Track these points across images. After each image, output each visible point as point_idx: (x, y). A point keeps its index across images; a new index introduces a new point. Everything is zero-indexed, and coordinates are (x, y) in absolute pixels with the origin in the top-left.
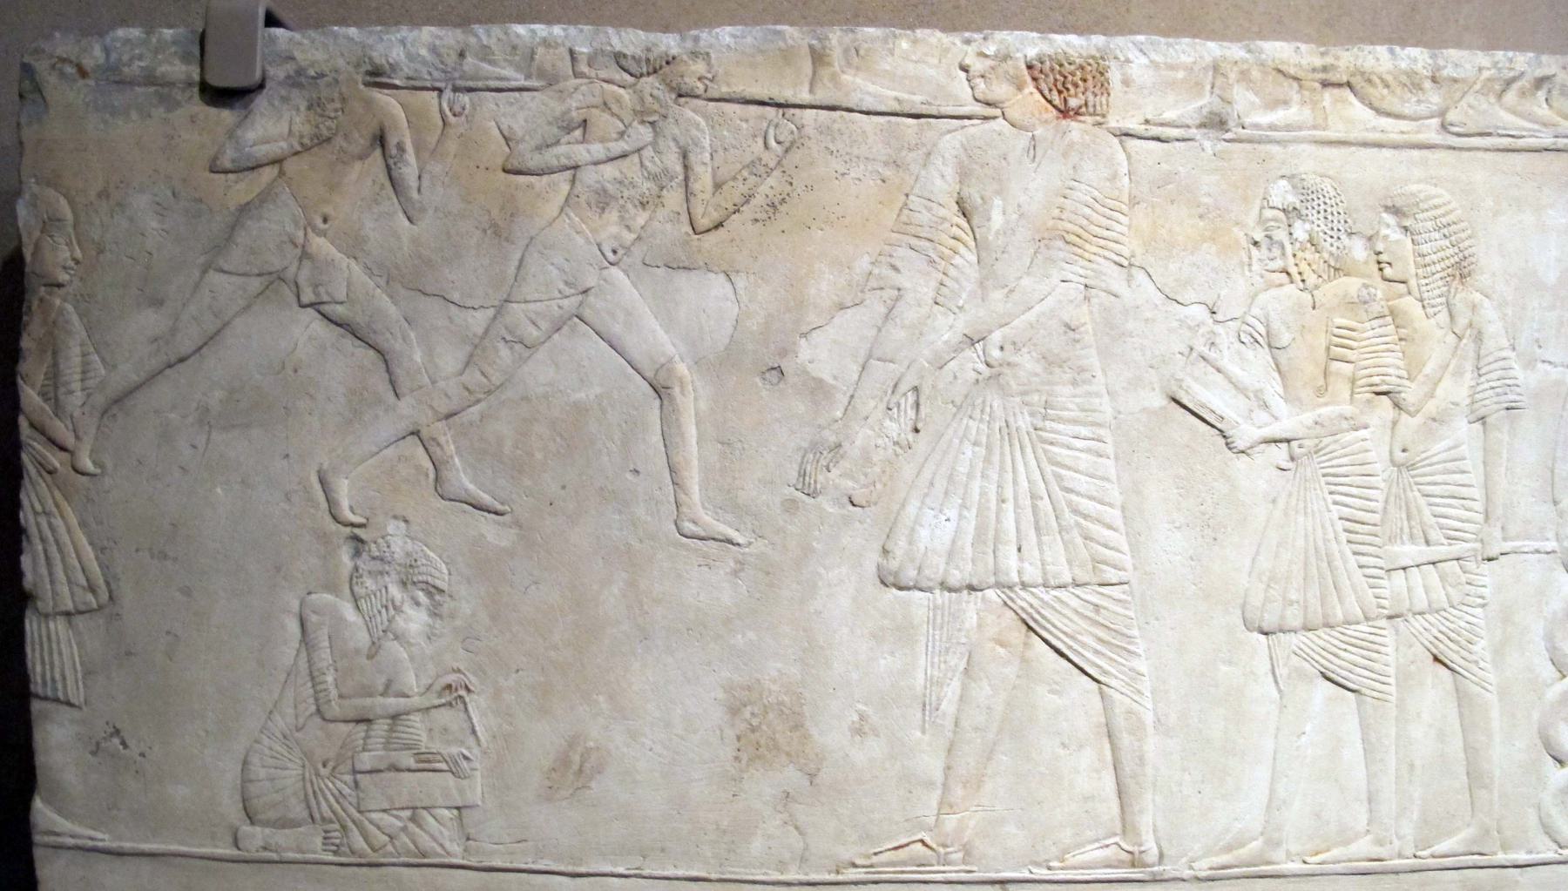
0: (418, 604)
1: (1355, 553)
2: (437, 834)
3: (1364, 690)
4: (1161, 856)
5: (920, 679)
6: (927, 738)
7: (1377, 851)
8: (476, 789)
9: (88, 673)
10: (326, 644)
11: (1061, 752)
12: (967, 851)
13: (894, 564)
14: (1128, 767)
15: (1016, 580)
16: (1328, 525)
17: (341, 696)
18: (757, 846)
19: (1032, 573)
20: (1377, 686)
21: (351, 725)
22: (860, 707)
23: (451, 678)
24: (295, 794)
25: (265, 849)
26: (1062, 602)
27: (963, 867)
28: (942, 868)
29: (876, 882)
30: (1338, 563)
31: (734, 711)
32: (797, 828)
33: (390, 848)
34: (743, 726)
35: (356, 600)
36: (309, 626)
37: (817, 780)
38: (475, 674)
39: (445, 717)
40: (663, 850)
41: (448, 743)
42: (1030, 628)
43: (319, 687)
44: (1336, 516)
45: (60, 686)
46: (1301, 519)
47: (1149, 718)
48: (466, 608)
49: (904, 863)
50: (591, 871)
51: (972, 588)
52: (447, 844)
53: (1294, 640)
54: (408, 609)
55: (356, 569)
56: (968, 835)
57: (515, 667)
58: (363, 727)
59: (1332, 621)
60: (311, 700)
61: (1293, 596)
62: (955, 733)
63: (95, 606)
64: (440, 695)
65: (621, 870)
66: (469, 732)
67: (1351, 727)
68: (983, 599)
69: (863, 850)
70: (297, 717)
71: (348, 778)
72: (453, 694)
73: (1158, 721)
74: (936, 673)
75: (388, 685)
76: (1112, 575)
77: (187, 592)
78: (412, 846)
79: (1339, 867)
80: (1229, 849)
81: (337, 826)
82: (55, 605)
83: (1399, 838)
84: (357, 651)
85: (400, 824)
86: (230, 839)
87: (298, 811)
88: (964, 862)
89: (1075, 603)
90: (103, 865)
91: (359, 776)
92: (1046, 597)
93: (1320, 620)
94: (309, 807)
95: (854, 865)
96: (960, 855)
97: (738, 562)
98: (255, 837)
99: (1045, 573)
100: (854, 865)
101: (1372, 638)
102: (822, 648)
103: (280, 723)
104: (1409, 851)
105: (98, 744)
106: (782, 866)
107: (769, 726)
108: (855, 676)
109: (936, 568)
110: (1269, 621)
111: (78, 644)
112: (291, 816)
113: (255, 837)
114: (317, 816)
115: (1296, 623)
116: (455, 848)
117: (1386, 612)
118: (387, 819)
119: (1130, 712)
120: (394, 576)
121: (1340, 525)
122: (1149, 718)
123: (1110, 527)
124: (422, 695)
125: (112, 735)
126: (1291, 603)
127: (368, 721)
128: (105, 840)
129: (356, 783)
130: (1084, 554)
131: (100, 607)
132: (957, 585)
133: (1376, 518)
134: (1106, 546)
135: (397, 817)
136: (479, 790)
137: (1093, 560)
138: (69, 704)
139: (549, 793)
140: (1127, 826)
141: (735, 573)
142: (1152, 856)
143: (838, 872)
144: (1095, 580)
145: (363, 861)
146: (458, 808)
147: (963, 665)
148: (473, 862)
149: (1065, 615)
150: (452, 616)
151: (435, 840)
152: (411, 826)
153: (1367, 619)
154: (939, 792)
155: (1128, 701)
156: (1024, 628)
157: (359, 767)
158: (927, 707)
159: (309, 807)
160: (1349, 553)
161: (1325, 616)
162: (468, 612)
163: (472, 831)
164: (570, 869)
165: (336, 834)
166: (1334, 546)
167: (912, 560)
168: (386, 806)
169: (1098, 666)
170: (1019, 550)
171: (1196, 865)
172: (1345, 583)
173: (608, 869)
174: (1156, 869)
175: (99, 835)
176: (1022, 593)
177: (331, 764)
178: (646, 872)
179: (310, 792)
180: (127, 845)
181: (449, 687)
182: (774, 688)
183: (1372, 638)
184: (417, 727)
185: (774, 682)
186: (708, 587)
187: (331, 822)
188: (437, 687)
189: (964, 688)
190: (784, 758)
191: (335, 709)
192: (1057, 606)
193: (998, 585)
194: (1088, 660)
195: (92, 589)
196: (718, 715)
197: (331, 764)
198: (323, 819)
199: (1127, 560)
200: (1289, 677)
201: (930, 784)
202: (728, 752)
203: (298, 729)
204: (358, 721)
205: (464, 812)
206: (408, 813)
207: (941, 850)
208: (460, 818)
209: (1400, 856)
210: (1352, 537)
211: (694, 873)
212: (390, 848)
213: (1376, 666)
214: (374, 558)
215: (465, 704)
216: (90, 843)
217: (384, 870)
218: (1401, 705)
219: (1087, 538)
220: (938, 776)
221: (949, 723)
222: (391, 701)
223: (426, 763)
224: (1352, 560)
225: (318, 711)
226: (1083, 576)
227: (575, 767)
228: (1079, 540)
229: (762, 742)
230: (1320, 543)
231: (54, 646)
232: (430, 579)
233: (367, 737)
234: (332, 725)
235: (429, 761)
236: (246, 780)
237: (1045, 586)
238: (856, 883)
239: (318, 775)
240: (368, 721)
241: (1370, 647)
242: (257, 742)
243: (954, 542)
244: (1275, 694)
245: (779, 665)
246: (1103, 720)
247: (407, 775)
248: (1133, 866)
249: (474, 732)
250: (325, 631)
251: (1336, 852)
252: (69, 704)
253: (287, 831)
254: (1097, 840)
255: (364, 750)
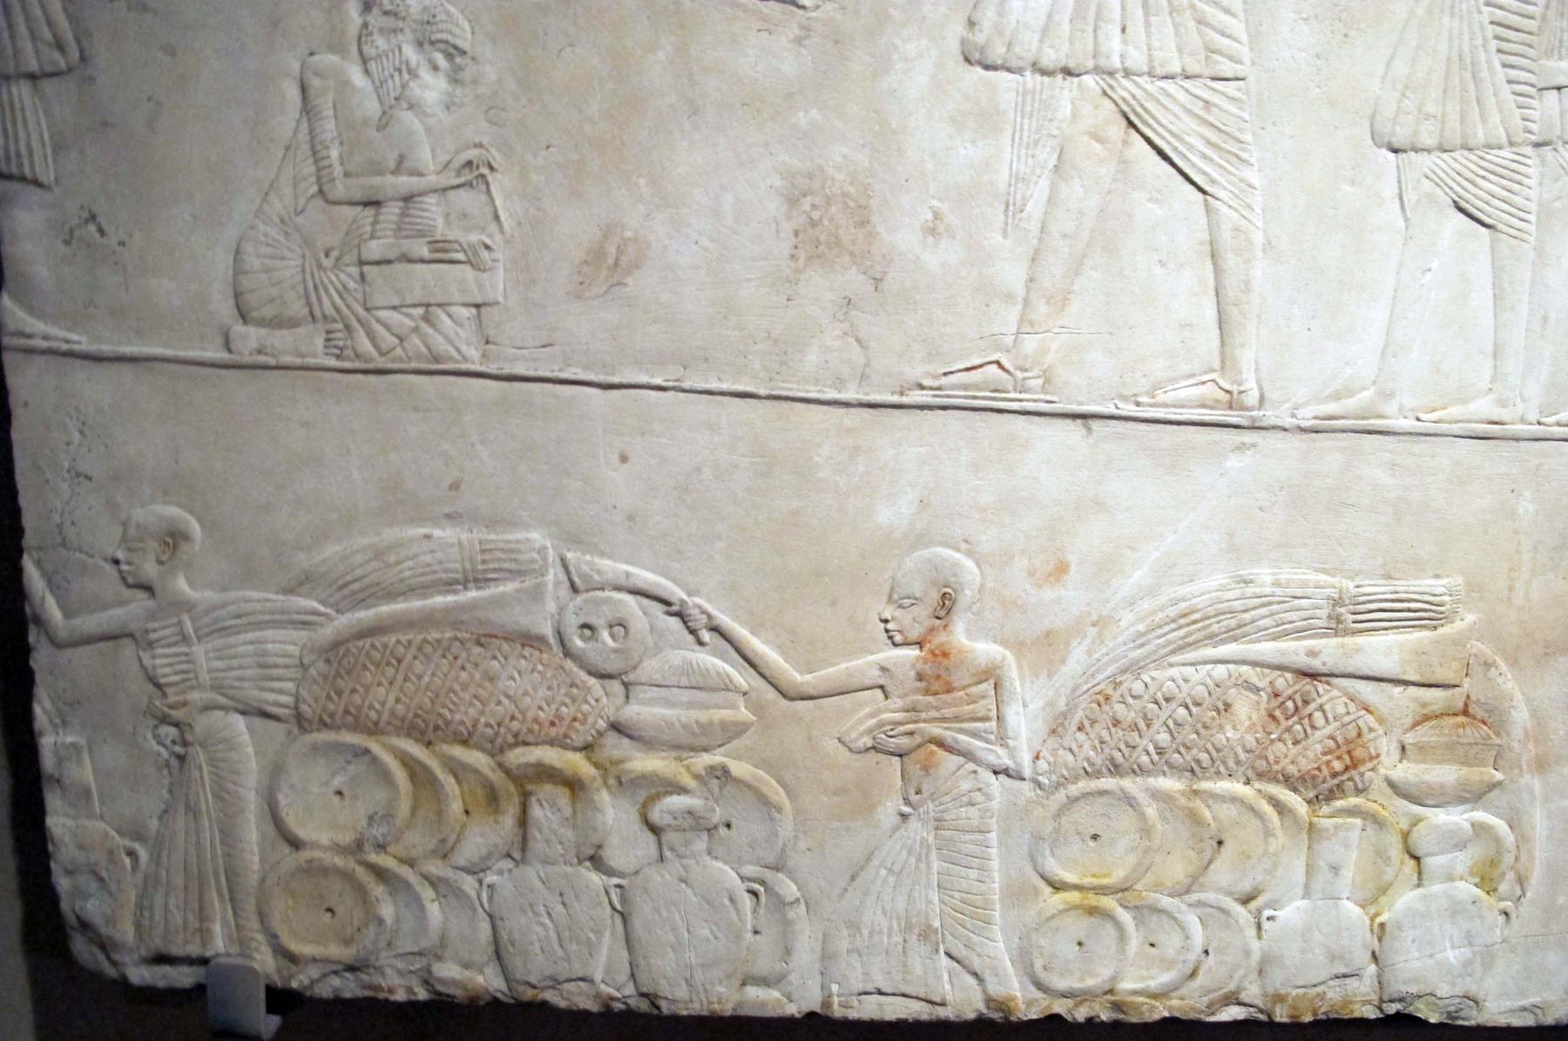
0: (435, 68)
1: (1504, 66)
2: (452, 335)
3: (1500, 226)
4: (1262, 399)
5: (1004, 175)
6: (1008, 243)
7: (1503, 414)
8: (497, 284)
9: (57, 150)
10: (331, 112)
11: (1158, 270)
12: (1048, 380)
13: (980, 38)
14: (1231, 293)
15: (1118, 65)
16: (1477, 30)
17: (347, 175)
18: (812, 358)
19: (1137, 60)
20: (1515, 222)
21: (360, 208)
22: (935, 203)
23: (472, 154)
24: (293, 287)
25: (260, 352)
26: (1169, 95)
27: (1042, 397)
28: (1019, 396)
29: (944, 408)
30: (1485, 74)
31: (792, 202)
32: (858, 340)
33: (399, 351)
34: (803, 219)
35: (365, 61)
36: (312, 92)
37: (884, 286)
38: (499, 150)
39: (465, 199)
40: (706, 360)
41: (468, 230)
42: (1131, 124)
43: (322, 164)
44: (1486, 20)
45: (26, 162)
46: (1446, 20)
47: (1258, 238)
48: (490, 73)
49: (977, 387)
50: (625, 381)
51: (1068, 72)
52: (464, 348)
53: (1425, 162)
54: (426, 75)
55: (365, 25)
56: (1049, 359)
57: (545, 144)
58: (370, 211)
59: (1472, 143)
60: (313, 179)
61: (1430, 108)
62: (1040, 240)
63: (63, 65)
64: (459, 173)
65: (658, 381)
66: (490, 217)
67: (1482, 270)
68: (1080, 86)
69: (930, 368)
70: (296, 198)
71: (354, 270)
72: (474, 174)
73: (1268, 245)
74: (1023, 169)
75: (401, 159)
76: (1227, 68)
77: (171, 51)
78: (423, 349)
79: (1455, 428)
80: (1337, 396)
81: (340, 326)
82: (17, 65)
83: (1523, 400)
84: (365, 123)
85: (412, 324)
86: (220, 341)
87: (297, 308)
88: (1044, 390)
89: (1182, 97)
90: (80, 374)
91: (366, 268)
92: (1149, 87)
93: (1458, 141)
94: (309, 304)
95: (922, 387)
96: (1040, 382)
97: (801, 27)
98: (250, 338)
99: (1151, 60)
100: (922, 387)
101: (1514, 166)
102: (894, 132)
103: (277, 206)
104: (1533, 417)
105: (71, 231)
106: (840, 383)
107: (831, 220)
108: (930, 166)
109: (1029, 45)
110: (1401, 137)
111: (46, 112)
112: (290, 313)
113: (250, 338)
114: (317, 313)
115: (1429, 141)
116: (473, 353)
117: (1533, 137)
118: (394, 317)
119: (1236, 229)
120: (409, 35)
121: (1491, 30)
122: (1258, 238)
123: (1227, 11)
124: (439, 173)
125: (87, 221)
126: (1428, 116)
127: (377, 204)
128: (82, 341)
129: (362, 275)
130: (1195, 40)
131: (70, 70)
132: (1051, 66)
133: (1532, 25)
134: (1223, 34)
135: (408, 316)
136: (501, 286)
137: (1207, 48)
138: (37, 183)
139: (580, 290)
140: (1226, 361)
141: (799, 41)
142: (1251, 399)
143: (902, 394)
144: (1207, 73)
145: (370, 366)
146: (477, 306)
147: (1053, 161)
148: (491, 368)
149: (1172, 115)
150: (475, 82)
151: (450, 342)
152: (423, 325)
153: (1511, 144)
154: (1020, 307)
155: (1236, 215)
156: (1124, 123)
157: (366, 256)
158: (1012, 208)
159: (309, 304)
160: (1497, 64)
161: (1464, 135)
162: (494, 77)
163: (492, 333)
164: (601, 378)
165: (339, 335)
166: (1483, 56)
167: (1001, 34)
168: (396, 302)
169: (1205, 173)
170: (1123, 30)
171: (1300, 413)
172: (1490, 101)
173: (643, 379)
174: (1255, 413)
175: (75, 337)
176: (1124, 82)
177: (335, 253)
178: (686, 385)
179: (310, 285)
180: (106, 348)
181: (469, 163)
182: (840, 176)
183: (1514, 166)
184: (433, 211)
185: (839, 169)
186: (769, 54)
187: (334, 321)
188: (456, 164)
189: (1053, 187)
190: (847, 258)
191: (339, 189)
192: (1163, 99)
193: (1098, 70)
194: (1194, 166)
195: (60, 46)
196: (774, 206)
197: (335, 253)
198: (325, 317)
199: (1245, 53)
200: (1418, 203)
201: (1009, 298)
202: (784, 248)
203: (297, 213)
204: (366, 204)
205: (483, 310)
206: (421, 311)
207: (1019, 375)
208: (479, 315)
209: (1523, 421)
210: (1504, 46)
211: (740, 388)
212: (399, 351)
213: (1518, 200)
214: (386, 13)
215: (487, 184)
216: (65, 347)
217: (391, 377)
218: (1540, 251)
219: (1201, 21)
220: (1019, 288)
221: (1034, 227)
222: (403, 180)
223: (442, 252)
224: (1501, 73)
225: (321, 191)
226: (1194, 68)
227: (611, 261)
228: (1192, 24)
229: (823, 238)
230: (1466, 49)
231: (19, 115)
232: (450, 38)
233: (376, 222)
234: (337, 208)
235: (446, 251)
236: (238, 269)
237: (1150, 74)
238: (922, 407)
239: (320, 266)
240: (377, 204)
241: (1511, 176)
242: (252, 227)
243: (1050, 16)
244: (1402, 224)
245: (845, 150)
246: (1207, 237)
247: (419, 266)
248: (1231, 408)
249: (497, 217)
250: (330, 97)
251: (1454, 411)
252: (37, 183)
253: (285, 332)
254: (1193, 376)
255: (372, 237)
